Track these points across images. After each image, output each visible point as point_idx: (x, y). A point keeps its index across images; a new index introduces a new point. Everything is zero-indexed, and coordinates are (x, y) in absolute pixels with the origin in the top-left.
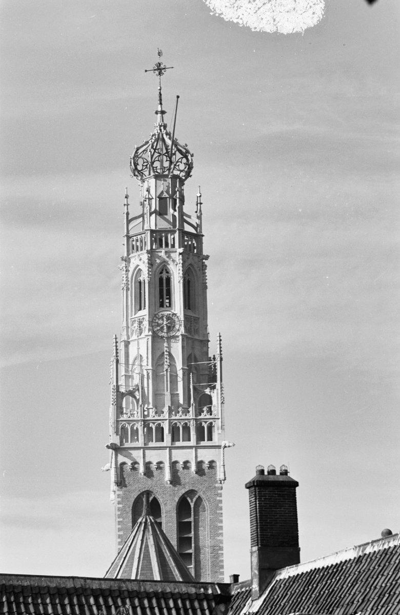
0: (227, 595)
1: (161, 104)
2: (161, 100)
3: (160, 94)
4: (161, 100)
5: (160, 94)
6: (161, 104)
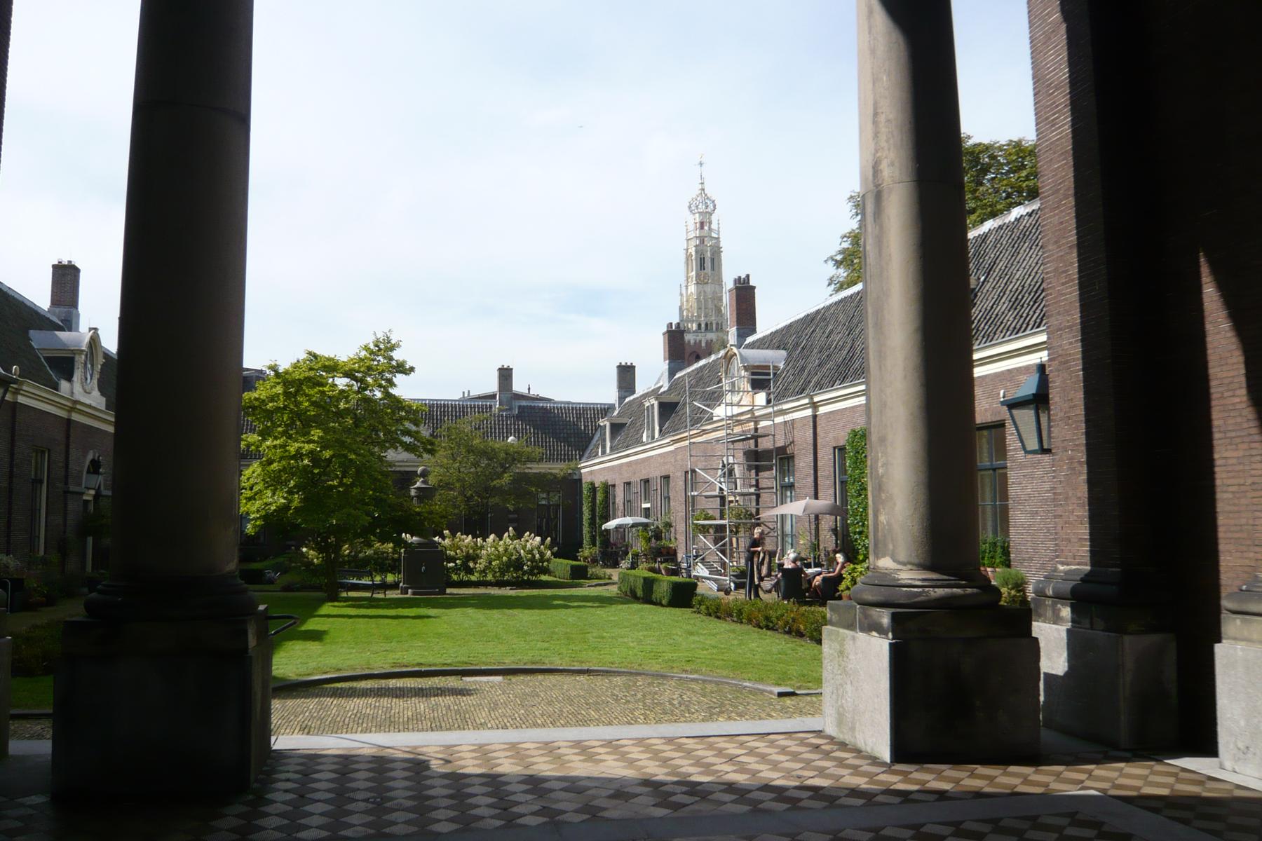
0: (1034, 618)
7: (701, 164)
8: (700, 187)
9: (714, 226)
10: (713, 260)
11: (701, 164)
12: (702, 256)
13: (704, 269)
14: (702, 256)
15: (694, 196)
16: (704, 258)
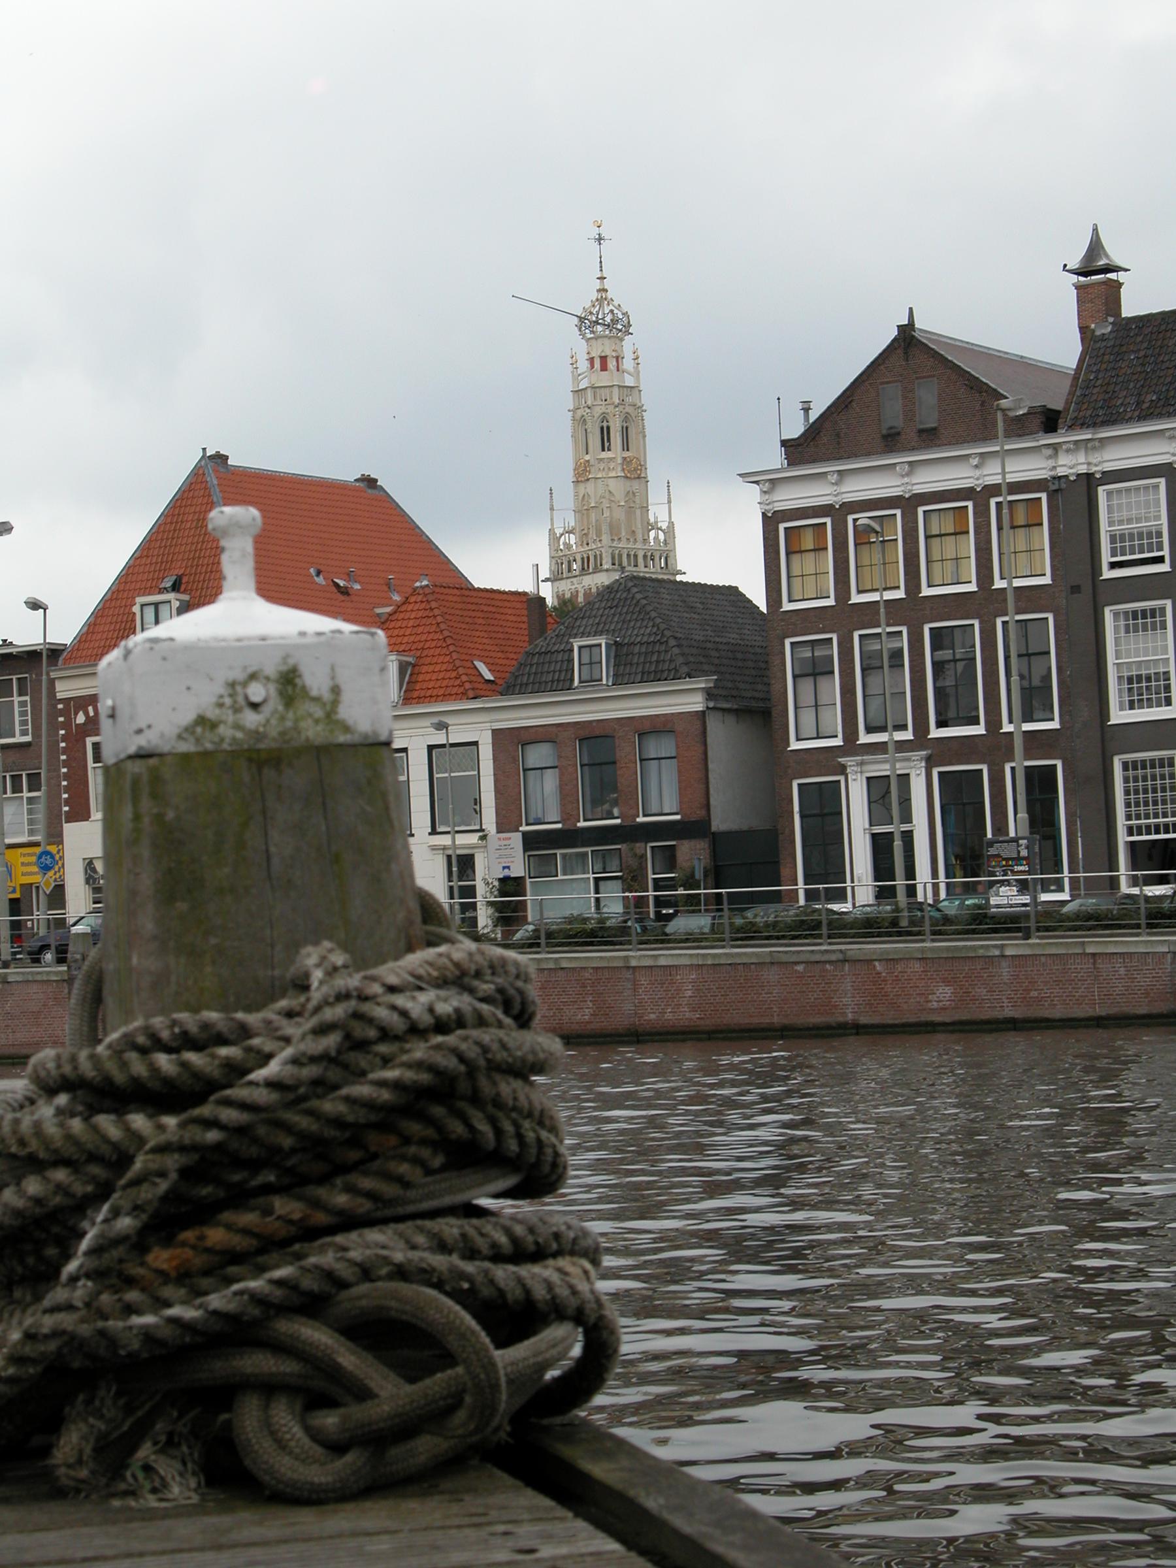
3: (601, 262)
5: (601, 262)
7: (600, 239)
8: (598, 285)
9: (628, 364)
10: (625, 431)
11: (600, 239)
12: (605, 424)
14: (605, 424)
15: (588, 305)
16: (608, 428)
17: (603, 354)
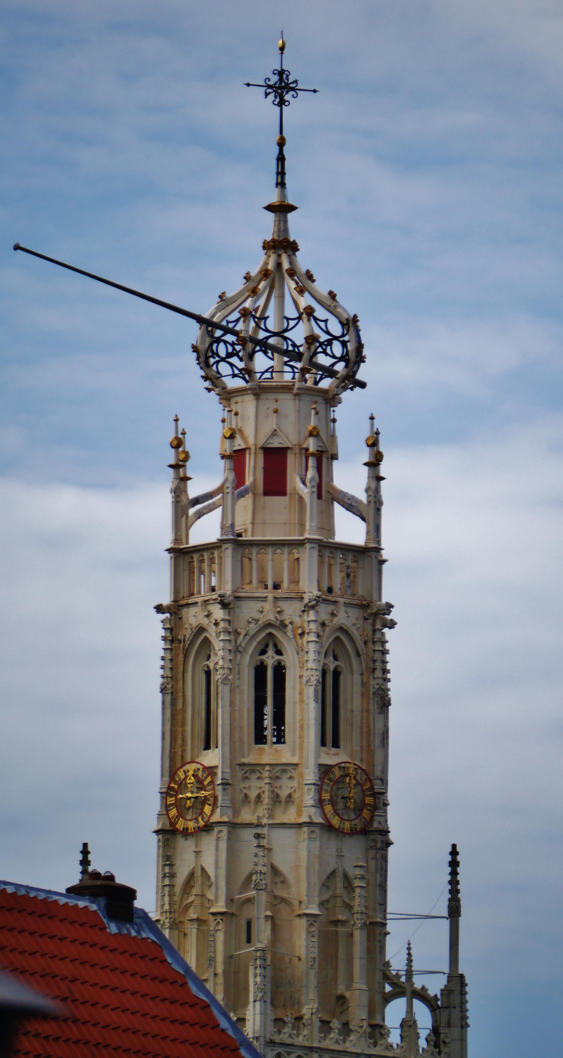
1: (281, 184)
2: (281, 173)
3: (281, 159)
4: (281, 173)
5: (281, 159)
6: (281, 184)
13: (280, 738)
17: (276, 443)
